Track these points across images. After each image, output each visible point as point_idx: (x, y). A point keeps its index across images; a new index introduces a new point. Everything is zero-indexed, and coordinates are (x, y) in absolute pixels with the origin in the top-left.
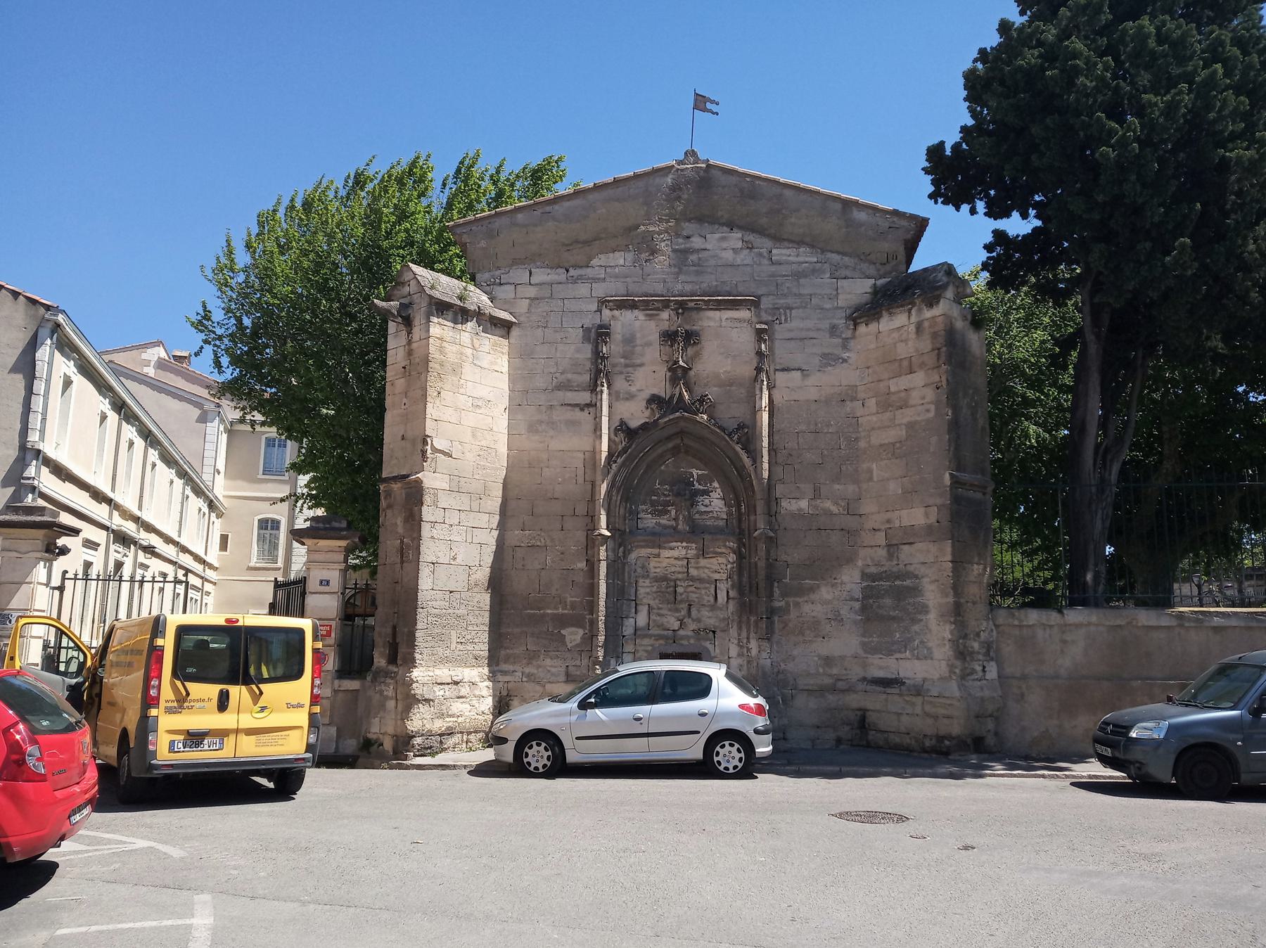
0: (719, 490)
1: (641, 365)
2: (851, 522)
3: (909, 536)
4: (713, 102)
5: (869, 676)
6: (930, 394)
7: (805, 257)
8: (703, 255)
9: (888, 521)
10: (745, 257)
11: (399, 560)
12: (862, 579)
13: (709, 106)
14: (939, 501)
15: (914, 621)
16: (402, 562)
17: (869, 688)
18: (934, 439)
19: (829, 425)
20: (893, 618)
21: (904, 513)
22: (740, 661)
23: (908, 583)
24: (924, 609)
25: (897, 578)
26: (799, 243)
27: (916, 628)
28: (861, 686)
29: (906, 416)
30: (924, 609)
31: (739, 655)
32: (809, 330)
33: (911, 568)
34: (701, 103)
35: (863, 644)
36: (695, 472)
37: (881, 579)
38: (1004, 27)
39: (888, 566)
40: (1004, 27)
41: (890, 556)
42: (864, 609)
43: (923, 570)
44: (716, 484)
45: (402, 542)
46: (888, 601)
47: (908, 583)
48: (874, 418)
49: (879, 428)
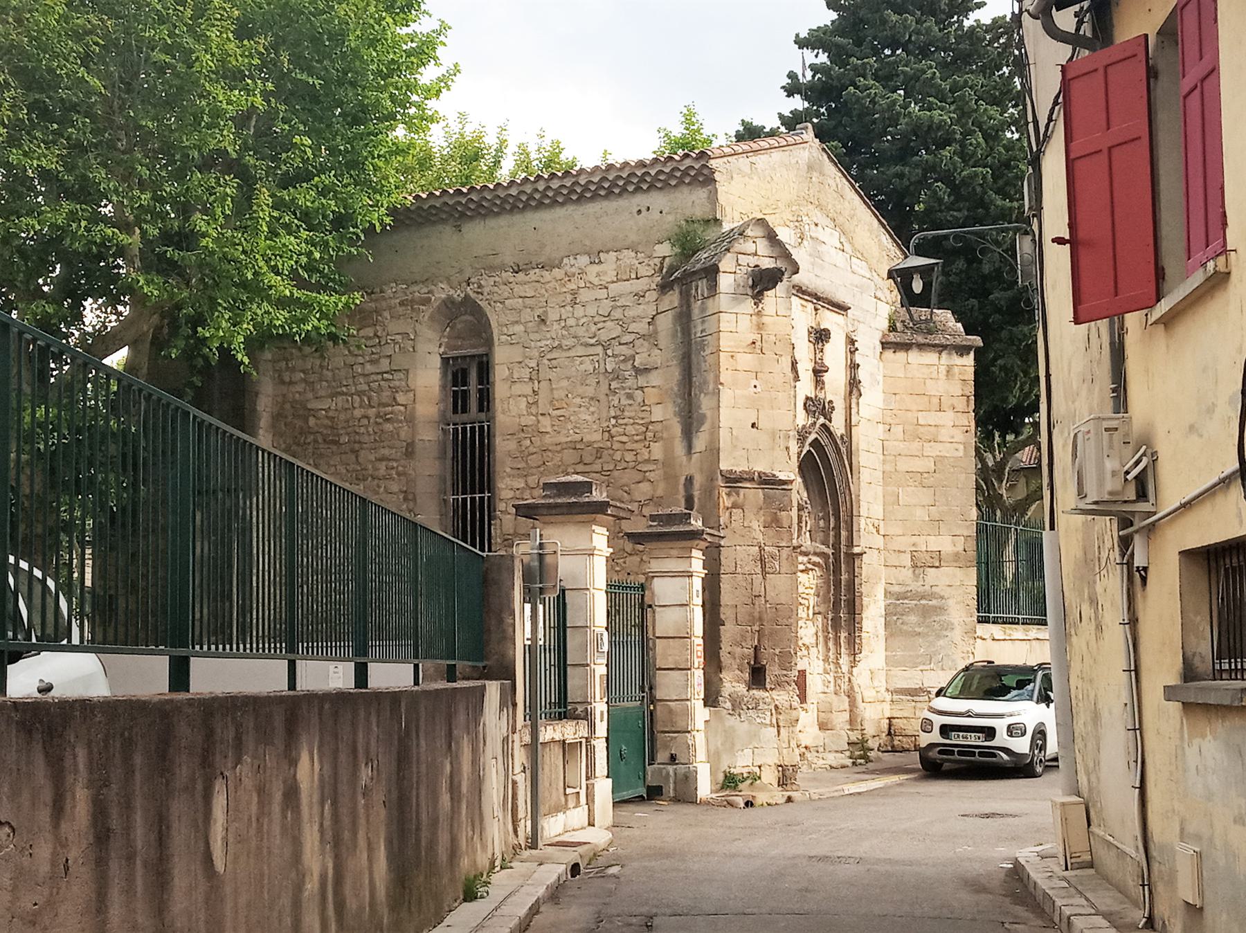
3: (937, 560)
6: (959, 436)
11: (759, 570)
15: (939, 637)
16: (764, 573)
17: (895, 697)
24: (949, 626)
25: (923, 598)
27: (941, 642)
30: (949, 626)
39: (915, 586)
43: (946, 592)
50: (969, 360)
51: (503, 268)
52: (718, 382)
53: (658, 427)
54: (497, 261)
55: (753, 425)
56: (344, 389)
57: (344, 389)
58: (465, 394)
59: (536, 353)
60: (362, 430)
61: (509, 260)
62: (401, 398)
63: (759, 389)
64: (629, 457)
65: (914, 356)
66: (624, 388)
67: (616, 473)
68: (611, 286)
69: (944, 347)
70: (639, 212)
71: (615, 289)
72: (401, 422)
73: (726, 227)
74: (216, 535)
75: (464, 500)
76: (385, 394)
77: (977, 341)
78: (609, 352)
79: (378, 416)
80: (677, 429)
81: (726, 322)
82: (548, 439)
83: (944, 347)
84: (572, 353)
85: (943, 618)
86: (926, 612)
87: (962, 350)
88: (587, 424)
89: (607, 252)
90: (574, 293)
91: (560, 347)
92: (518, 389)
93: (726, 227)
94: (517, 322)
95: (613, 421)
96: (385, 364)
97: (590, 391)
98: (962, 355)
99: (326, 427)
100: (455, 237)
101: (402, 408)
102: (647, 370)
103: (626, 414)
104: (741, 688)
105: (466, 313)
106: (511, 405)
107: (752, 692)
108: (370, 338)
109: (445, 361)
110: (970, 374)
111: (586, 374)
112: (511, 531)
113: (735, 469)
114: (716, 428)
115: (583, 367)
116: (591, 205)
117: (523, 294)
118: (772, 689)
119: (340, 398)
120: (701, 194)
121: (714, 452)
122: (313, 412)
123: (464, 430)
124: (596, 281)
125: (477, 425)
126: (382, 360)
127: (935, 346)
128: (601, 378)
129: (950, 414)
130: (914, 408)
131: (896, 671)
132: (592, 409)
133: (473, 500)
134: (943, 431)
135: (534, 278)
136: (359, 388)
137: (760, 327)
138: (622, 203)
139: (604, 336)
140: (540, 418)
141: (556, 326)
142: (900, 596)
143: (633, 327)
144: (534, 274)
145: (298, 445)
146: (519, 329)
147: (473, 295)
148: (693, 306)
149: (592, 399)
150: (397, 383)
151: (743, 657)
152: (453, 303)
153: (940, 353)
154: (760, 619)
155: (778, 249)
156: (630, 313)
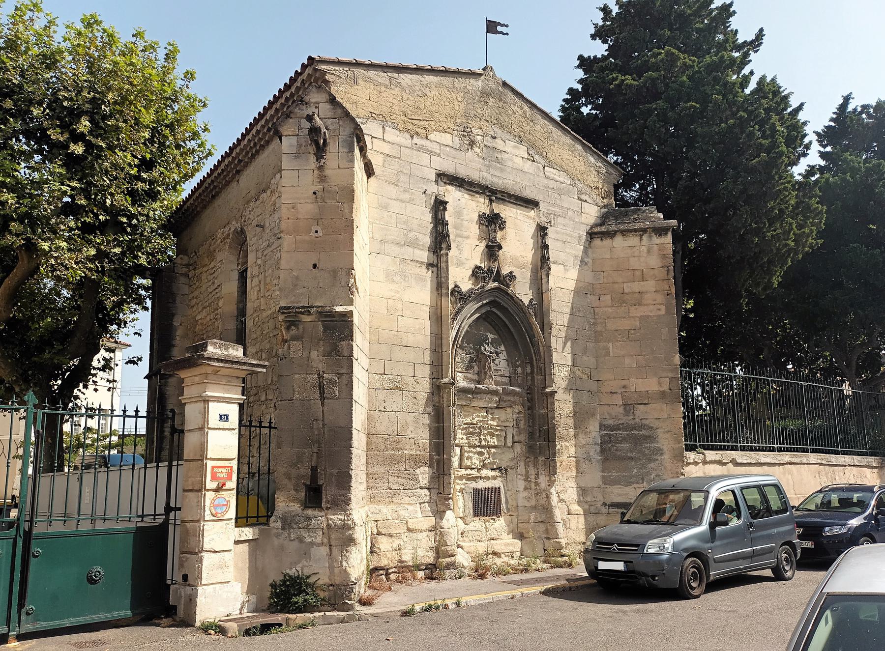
0: (505, 353)
1: (467, 237)
2: (593, 386)
3: (645, 399)
4: (503, 25)
5: (608, 502)
6: (660, 298)
7: (562, 177)
8: (504, 156)
9: (624, 387)
10: (528, 166)
11: (317, 396)
12: (601, 429)
13: (499, 28)
14: (670, 375)
15: (650, 460)
16: (323, 398)
17: (611, 510)
18: (665, 331)
19: (579, 311)
20: (632, 458)
21: (639, 381)
22: (526, 494)
23: (644, 432)
24: (660, 452)
25: (634, 429)
26: (562, 169)
27: (652, 465)
28: (604, 510)
29: (641, 311)
30: (660, 452)
31: (526, 489)
32: (567, 234)
33: (644, 422)
34: (492, 27)
35: (603, 477)
36: (490, 336)
37: (619, 429)
38: (585, 63)
39: (624, 420)
40: (585, 63)
41: (627, 413)
42: (603, 451)
43: (656, 424)
44: (502, 348)
45: (320, 377)
46: (626, 446)
47: (644, 432)
48: (610, 310)
49: (615, 318)
50: (669, 238)
55: (315, 266)
63: (320, 234)
65: (619, 240)
69: (644, 231)
81: (288, 178)
83: (644, 231)
85: (653, 445)
86: (637, 441)
87: (660, 231)
98: (660, 235)
104: (296, 507)
107: (305, 512)
110: (670, 248)
118: (327, 509)
127: (635, 231)
130: (620, 280)
131: (609, 488)
134: (646, 296)
137: (323, 179)
142: (612, 428)
151: (299, 477)
153: (641, 236)
154: (319, 442)
155: (339, 111)
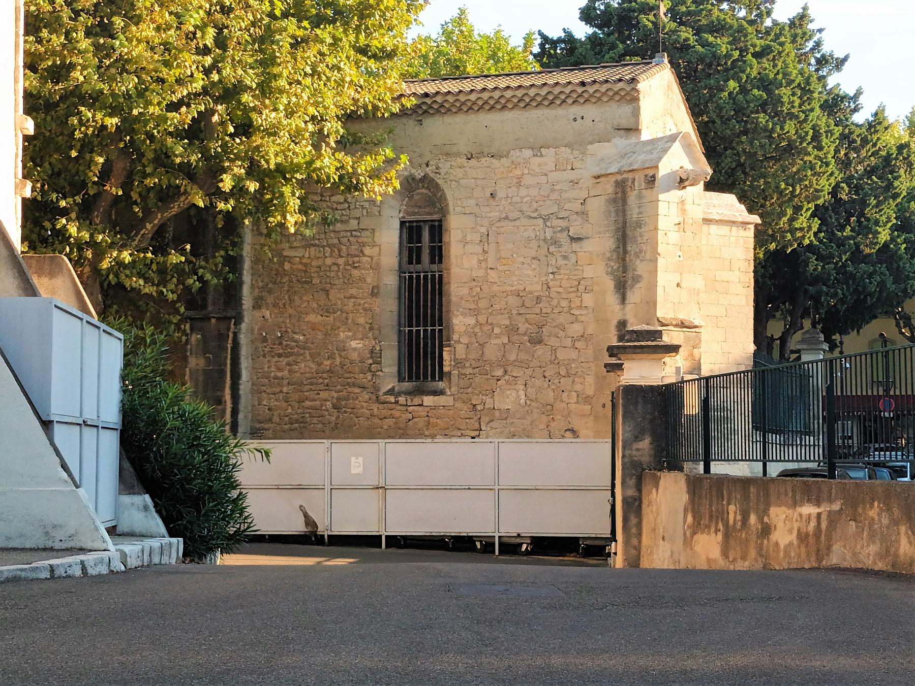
51: (458, 154)
52: (655, 253)
53: (589, 283)
54: (454, 149)
55: (678, 285)
56: (317, 242)
57: (317, 242)
58: (419, 249)
59: (486, 222)
60: (333, 274)
61: (464, 149)
62: (367, 251)
64: (564, 304)
66: (560, 252)
67: (552, 316)
68: (550, 174)
70: (575, 120)
71: (554, 176)
72: (367, 269)
73: (645, 136)
74: (846, 368)
75: (410, 332)
76: (353, 247)
77: (756, 219)
78: (548, 224)
79: (347, 264)
80: (610, 284)
82: (495, 288)
84: (517, 223)
88: (529, 277)
89: (548, 148)
90: (519, 178)
91: (507, 218)
92: (469, 249)
93: (645, 136)
94: (470, 197)
95: (551, 276)
96: (353, 224)
97: (533, 253)
99: (300, 270)
100: (417, 128)
101: (369, 259)
102: (579, 239)
103: (562, 271)
105: (423, 187)
106: (463, 261)
108: (341, 203)
109: (402, 223)
111: (529, 239)
112: (464, 356)
113: (666, 316)
114: (653, 286)
115: (526, 234)
116: (535, 111)
117: (475, 176)
119: (312, 249)
120: (626, 109)
121: (651, 303)
122: (289, 259)
123: (418, 277)
124: (537, 170)
125: (429, 274)
126: (352, 221)
128: (542, 243)
129: (737, 273)
132: (533, 266)
133: (425, 331)
135: (486, 164)
136: (330, 242)
138: (560, 111)
139: (544, 212)
140: (489, 271)
141: (503, 202)
143: (567, 206)
144: (485, 161)
145: (275, 283)
146: (472, 202)
147: (432, 175)
148: (629, 193)
149: (534, 258)
150: (365, 240)
152: (414, 179)
156: (564, 195)
